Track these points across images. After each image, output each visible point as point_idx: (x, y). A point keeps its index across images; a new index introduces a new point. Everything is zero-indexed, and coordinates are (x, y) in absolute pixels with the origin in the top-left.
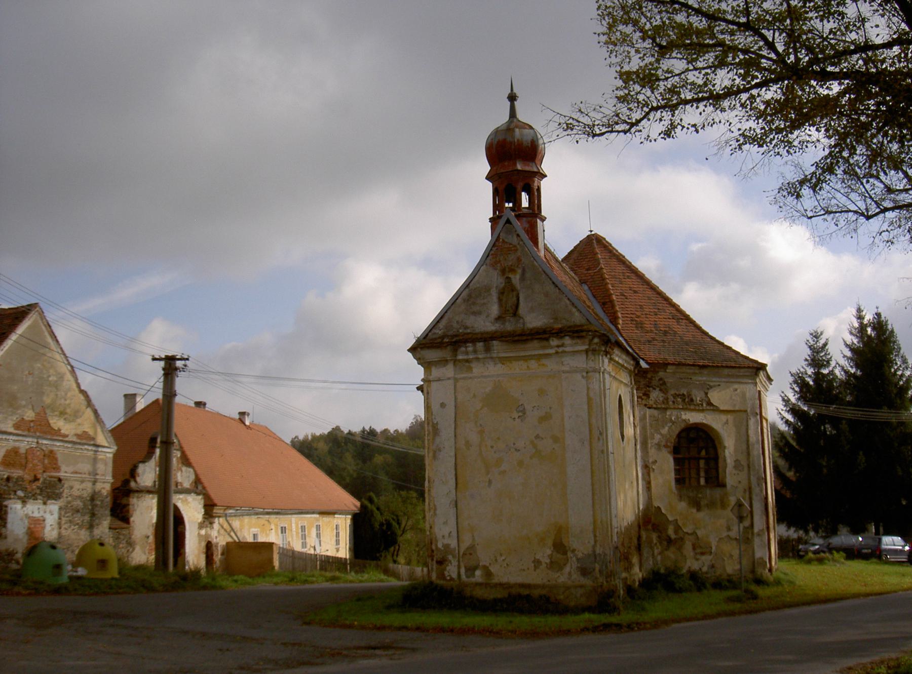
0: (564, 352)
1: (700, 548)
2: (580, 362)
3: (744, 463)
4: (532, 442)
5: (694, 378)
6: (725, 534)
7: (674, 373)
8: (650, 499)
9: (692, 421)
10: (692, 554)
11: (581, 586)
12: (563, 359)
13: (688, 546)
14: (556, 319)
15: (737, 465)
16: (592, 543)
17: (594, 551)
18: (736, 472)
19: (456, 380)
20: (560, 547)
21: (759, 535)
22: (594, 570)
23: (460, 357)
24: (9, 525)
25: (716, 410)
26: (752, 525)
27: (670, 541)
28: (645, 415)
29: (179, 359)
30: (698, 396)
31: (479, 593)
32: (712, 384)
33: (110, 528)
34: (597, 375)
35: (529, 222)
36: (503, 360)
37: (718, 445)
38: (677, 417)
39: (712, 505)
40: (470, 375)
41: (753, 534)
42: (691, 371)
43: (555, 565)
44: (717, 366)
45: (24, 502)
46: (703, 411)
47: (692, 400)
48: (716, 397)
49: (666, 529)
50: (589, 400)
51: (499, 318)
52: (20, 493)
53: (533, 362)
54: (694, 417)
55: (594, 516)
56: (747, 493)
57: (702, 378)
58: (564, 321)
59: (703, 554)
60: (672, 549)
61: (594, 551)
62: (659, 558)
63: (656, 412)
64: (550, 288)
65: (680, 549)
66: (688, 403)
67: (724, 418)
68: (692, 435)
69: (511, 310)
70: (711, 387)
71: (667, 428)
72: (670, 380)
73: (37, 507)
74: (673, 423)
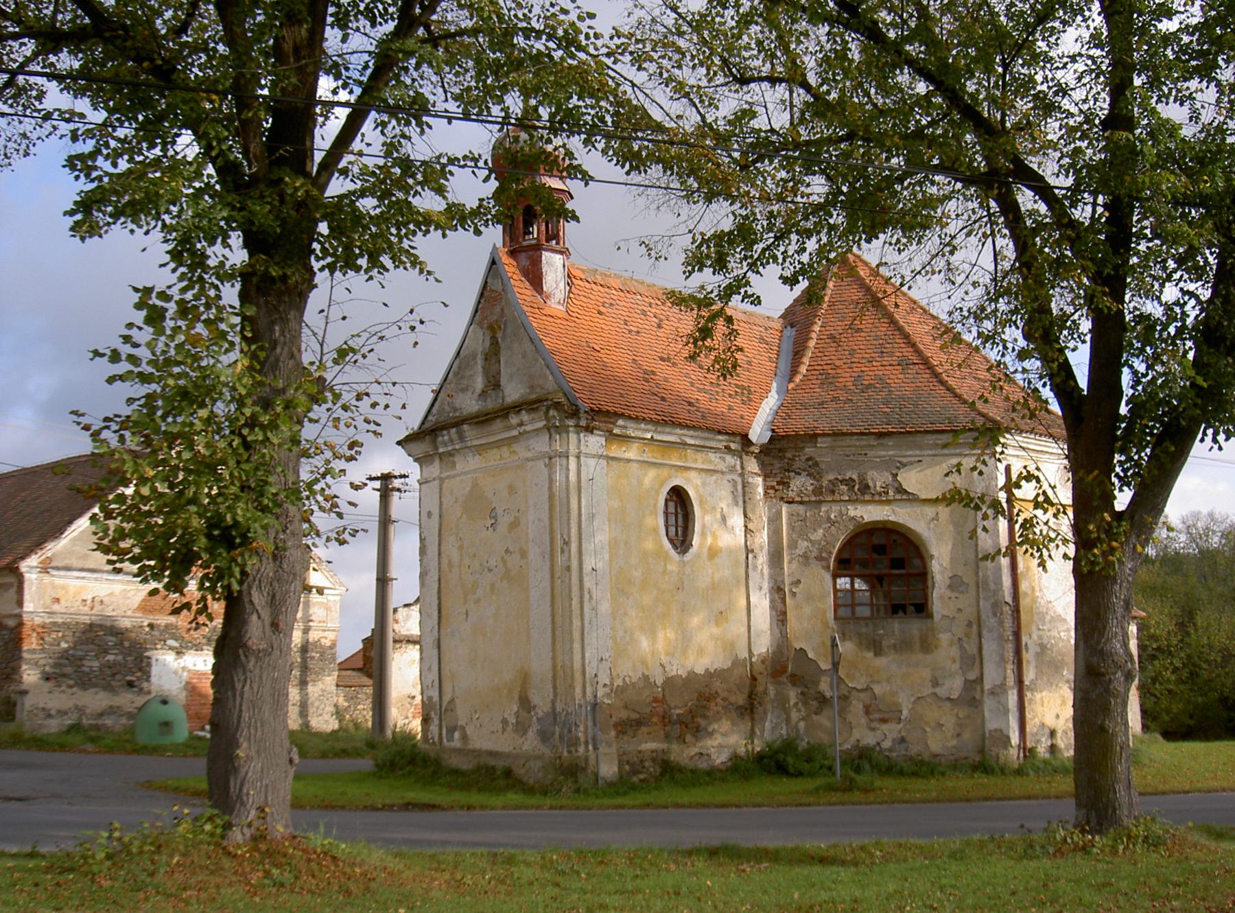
0: (526, 432)
1: (880, 712)
2: (541, 444)
3: (968, 578)
4: (502, 558)
5: (871, 453)
6: (927, 690)
7: (832, 448)
8: (784, 636)
9: (867, 519)
10: (863, 721)
11: (539, 757)
12: (530, 442)
13: (857, 707)
14: (532, 387)
15: (956, 583)
16: (551, 696)
17: (554, 709)
18: (953, 595)
19: (442, 480)
20: (525, 703)
21: (992, 693)
22: (553, 734)
23: (441, 450)
24: (154, 679)
25: (912, 499)
26: (980, 679)
27: (823, 701)
28: (779, 513)
29: (396, 477)
30: (878, 479)
31: (455, 762)
32: (904, 460)
33: (337, 686)
34: (564, 461)
35: (530, 258)
36: (480, 449)
37: (925, 555)
38: (841, 515)
39: (904, 646)
40: (453, 473)
41: (982, 691)
42: (864, 443)
43: (521, 728)
44: (909, 432)
45: (179, 653)
46: (888, 502)
47: (867, 487)
48: (911, 480)
49: (817, 683)
50: (551, 497)
51: (483, 394)
52: (171, 642)
53: (505, 449)
54: (871, 513)
55: (554, 658)
56: (975, 627)
57: (888, 451)
58: (538, 390)
59: (884, 721)
60: (827, 712)
61: (554, 709)
62: (802, 725)
63: (801, 509)
64: (527, 345)
65: (842, 712)
66: (862, 491)
67: (930, 511)
68: (876, 540)
69: (494, 384)
70: (904, 465)
71: (821, 531)
72: (825, 459)
73: (202, 659)
74: (833, 523)
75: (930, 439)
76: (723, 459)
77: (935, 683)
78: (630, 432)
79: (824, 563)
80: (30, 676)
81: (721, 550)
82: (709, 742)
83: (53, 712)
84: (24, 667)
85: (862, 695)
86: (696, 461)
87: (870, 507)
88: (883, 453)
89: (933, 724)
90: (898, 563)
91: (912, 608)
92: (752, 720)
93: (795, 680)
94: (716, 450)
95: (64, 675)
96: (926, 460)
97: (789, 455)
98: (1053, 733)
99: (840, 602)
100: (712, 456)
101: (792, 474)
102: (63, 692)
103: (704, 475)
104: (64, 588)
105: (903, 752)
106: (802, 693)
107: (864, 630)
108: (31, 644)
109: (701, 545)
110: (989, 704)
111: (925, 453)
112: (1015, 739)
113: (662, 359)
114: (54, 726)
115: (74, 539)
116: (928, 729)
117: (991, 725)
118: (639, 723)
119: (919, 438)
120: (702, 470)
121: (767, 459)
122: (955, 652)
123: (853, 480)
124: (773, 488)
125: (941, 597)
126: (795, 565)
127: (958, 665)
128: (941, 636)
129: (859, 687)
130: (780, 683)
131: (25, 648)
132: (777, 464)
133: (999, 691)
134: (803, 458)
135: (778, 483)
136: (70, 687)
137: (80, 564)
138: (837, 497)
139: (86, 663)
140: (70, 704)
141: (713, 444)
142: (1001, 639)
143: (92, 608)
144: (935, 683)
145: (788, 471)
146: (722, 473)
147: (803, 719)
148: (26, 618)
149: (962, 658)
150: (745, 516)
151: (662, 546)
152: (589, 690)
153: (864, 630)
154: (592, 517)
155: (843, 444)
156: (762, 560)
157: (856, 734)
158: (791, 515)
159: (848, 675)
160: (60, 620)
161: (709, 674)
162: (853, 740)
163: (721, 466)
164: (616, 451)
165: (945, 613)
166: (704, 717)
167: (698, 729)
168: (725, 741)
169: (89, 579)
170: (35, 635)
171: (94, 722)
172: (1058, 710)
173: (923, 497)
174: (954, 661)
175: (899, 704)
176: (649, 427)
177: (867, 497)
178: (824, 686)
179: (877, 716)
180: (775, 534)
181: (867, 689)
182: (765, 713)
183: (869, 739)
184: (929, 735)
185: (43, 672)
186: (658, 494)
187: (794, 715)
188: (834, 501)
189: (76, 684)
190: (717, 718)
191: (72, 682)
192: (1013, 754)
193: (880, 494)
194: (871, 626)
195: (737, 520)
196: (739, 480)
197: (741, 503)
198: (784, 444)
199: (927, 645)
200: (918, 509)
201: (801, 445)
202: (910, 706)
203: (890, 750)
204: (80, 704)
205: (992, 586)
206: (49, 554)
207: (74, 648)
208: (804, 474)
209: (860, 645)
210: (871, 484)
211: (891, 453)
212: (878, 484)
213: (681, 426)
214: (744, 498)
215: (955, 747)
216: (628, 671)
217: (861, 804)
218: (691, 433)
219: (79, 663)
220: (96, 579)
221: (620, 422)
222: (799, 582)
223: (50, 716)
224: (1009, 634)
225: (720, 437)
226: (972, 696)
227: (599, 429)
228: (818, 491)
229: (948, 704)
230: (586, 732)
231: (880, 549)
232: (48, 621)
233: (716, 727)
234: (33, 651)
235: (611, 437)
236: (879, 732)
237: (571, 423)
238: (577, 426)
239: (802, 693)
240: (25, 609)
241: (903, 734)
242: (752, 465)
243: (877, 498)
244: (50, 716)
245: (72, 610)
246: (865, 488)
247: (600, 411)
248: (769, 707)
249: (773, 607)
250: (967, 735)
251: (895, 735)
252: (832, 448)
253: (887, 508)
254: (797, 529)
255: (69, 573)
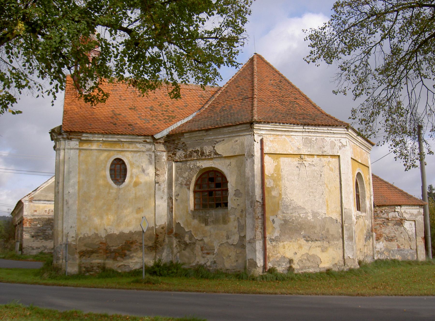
1: (207, 250)
5: (205, 138)
6: (225, 241)
7: (190, 138)
10: (200, 253)
13: (198, 247)
15: (237, 193)
18: (236, 198)
26: (245, 237)
30: (207, 149)
32: (218, 140)
39: (216, 221)
42: (201, 134)
46: (212, 159)
47: (203, 153)
48: (220, 149)
49: (184, 237)
54: (205, 164)
57: (211, 137)
59: (208, 254)
63: (180, 164)
65: (193, 250)
66: (202, 155)
67: (227, 161)
70: (217, 142)
71: (187, 173)
72: (188, 142)
75: (226, 130)
76: (145, 147)
77: (228, 238)
78: (122, 140)
79: (188, 186)
80: (26, 236)
81: (141, 183)
82: (130, 261)
83: (35, 248)
84: (24, 233)
85: (200, 242)
86: (129, 148)
87: (205, 162)
88: (210, 138)
89: (226, 256)
90: (218, 185)
91: (224, 204)
92: (156, 252)
93: (176, 235)
94: (140, 143)
95: (39, 236)
96: (226, 139)
97: (176, 142)
98: (291, 261)
99: (196, 203)
100: (138, 145)
101: (177, 150)
102: (38, 241)
103: (133, 153)
104: (38, 207)
105: (215, 268)
106: (179, 241)
107: (201, 214)
108: (27, 225)
109: (130, 182)
110: (248, 247)
111: (225, 136)
112: (260, 263)
113: (130, 109)
114: (35, 252)
115: (42, 191)
116: (225, 258)
117: (249, 257)
118: (92, 252)
119: (222, 130)
120: (132, 151)
121: (167, 144)
122: (236, 224)
123: (199, 151)
124: (170, 156)
125: (231, 199)
126: (177, 188)
127: (237, 229)
128: (231, 216)
129: (199, 239)
130: (171, 237)
131: (24, 227)
132: (172, 146)
133: (253, 241)
134: (181, 143)
135: (173, 154)
136: (41, 239)
137: (44, 199)
138: (192, 158)
139: (47, 231)
140: (41, 245)
141: (137, 140)
142: (254, 218)
143: (49, 213)
144: (228, 238)
145: (176, 149)
146: (143, 152)
147: (179, 252)
148: (24, 217)
149: (239, 226)
150: (155, 168)
151: (108, 183)
152: (65, 238)
153: (201, 214)
154: (69, 172)
155: (194, 135)
156: (164, 186)
157: (198, 259)
158: (177, 167)
159: (195, 234)
160: (37, 218)
161: (131, 233)
162: (196, 262)
163: (144, 149)
164: (85, 146)
165: (232, 206)
166: (129, 250)
167: (125, 255)
168: (138, 260)
169: (47, 204)
170: (28, 222)
171: (50, 251)
172: (296, 251)
173: (224, 156)
174: (236, 228)
175: (214, 247)
176: (100, 136)
177: (203, 157)
178: (187, 239)
179: (206, 251)
180: (170, 175)
181: (202, 240)
182: (163, 249)
183: (202, 262)
184: (225, 260)
185: (31, 235)
186: (107, 162)
187: (175, 251)
188: (191, 160)
189: (43, 239)
190: (136, 251)
191: (42, 238)
192: (259, 271)
193: (208, 156)
194: (204, 213)
195: (151, 170)
196: (153, 154)
197: (154, 163)
198: (174, 138)
199: (225, 221)
200: (223, 161)
201: (179, 138)
202: (218, 247)
203: (210, 267)
204: (45, 245)
205: (251, 194)
206: (33, 196)
207: (42, 227)
208: (181, 149)
209: (200, 221)
210: (205, 152)
211: (212, 138)
212: (207, 151)
213: (118, 134)
214: (156, 161)
215: (235, 266)
216: (86, 231)
217: (143, 289)
218: (123, 136)
219: (44, 231)
220: (50, 204)
221: (84, 135)
222: (178, 195)
223: (33, 249)
224: (259, 215)
225: (140, 137)
226: (242, 245)
227: (73, 138)
228: (186, 157)
229: (233, 247)
230: (62, 255)
231: (212, 180)
232: (32, 218)
233: (135, 254)
234: (27, 228)
235: (82, 141)
236: (206, 259)
237: (60, 137)
238: (63, 138)
239: (179, 241)
240: (24, 214)
241: (215, 260)
242: (161, 147)
243: (207, 157)
244: (33, 249)
245: (41, 214)
246: (203, 154)
247: (71, 132)
248: (166, 247)
249: (168, 206)
250: (240, 261)
251: (212, 260)
252: (190, 138)
253: (211, 161)
254: (179, 173)
255: (40, 202)
